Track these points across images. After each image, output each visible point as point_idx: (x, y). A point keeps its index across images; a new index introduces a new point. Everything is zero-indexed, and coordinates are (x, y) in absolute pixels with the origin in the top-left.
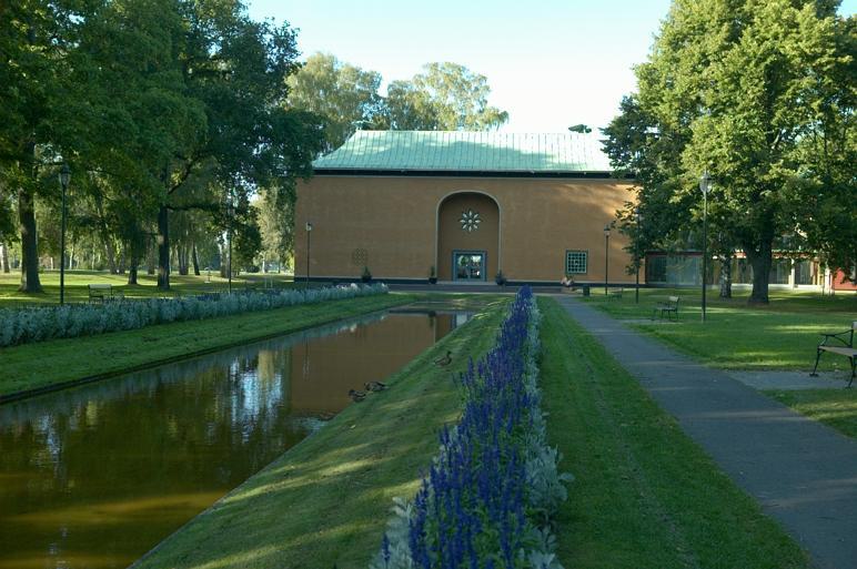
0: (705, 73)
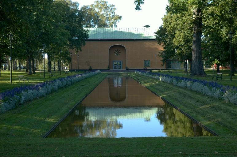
0: (178, 21)
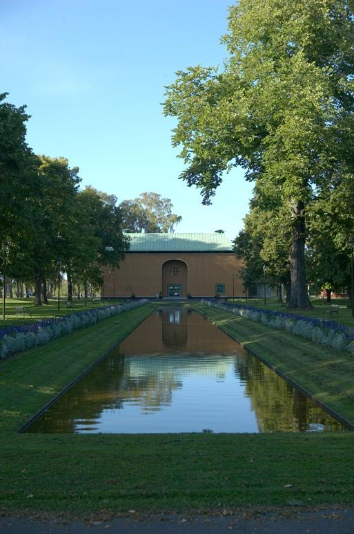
0: (267, 224)
